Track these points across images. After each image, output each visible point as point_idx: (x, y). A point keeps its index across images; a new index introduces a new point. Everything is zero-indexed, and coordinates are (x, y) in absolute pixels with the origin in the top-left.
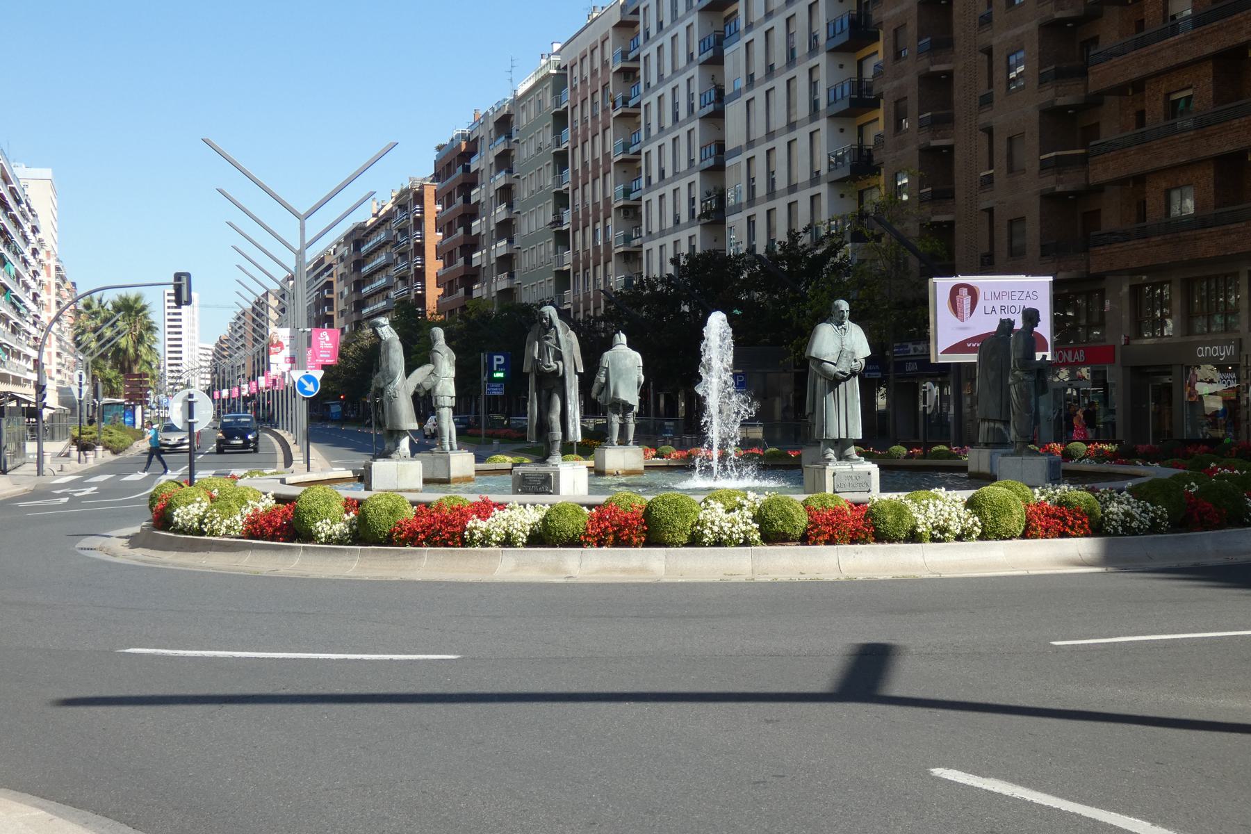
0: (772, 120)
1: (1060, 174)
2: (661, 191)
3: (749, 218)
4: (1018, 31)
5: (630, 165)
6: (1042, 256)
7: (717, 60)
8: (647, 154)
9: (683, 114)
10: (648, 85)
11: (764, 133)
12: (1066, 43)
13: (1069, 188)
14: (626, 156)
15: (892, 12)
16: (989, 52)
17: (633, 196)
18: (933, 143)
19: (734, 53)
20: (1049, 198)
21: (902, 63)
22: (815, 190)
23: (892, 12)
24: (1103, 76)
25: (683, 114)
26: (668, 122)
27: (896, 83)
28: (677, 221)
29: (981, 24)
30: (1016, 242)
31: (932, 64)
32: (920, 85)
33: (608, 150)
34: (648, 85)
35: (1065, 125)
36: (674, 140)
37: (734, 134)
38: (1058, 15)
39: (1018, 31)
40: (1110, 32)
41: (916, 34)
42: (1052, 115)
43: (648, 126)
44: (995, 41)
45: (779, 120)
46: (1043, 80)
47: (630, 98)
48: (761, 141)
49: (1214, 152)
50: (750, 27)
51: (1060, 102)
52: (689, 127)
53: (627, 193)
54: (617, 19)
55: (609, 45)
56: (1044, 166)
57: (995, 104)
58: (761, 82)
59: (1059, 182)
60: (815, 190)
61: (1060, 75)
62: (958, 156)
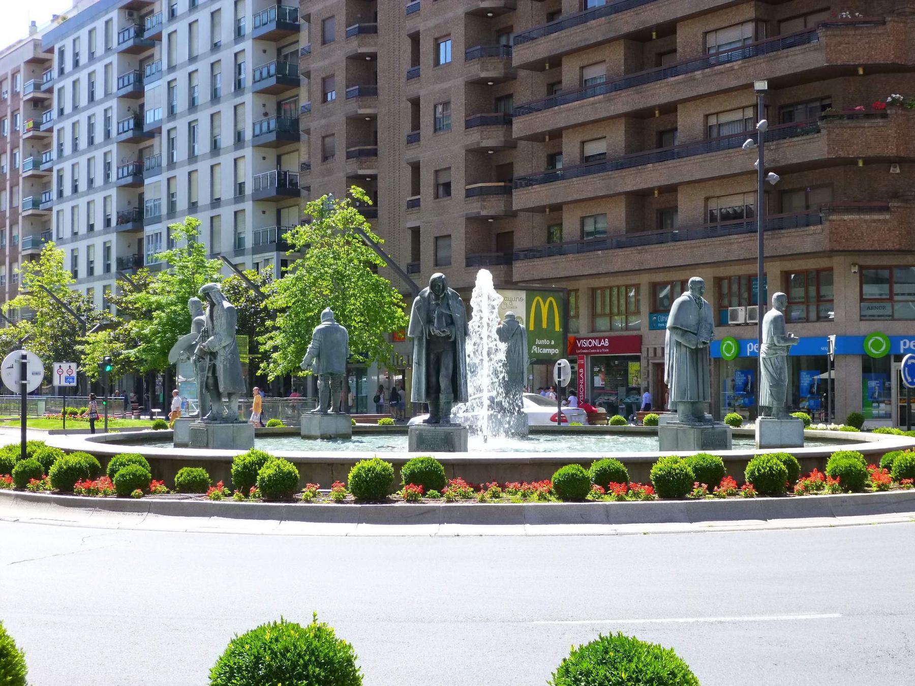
0: (195, 46)
1: (484, 201)
2: (75, 119)
3: (169, 83)
4: (446, 85)
5: (39, 181)
6: (467, 197)
7: (138, 93)
8: (60, 90)
9: (99, 137)
10: (61, 112)
11: (187, 58)
12: (489, 30)
13: (492, 213)
14: (36, 172)
15: (321, 64)
16: (415, 38)
17: (43, 167)
18: (361, 172)
19: (154, 90)
20: (473, 220)
21: (330, 106)
22: (239, 207)
23: (321, 64)
24: (522, 55)
25: (99, 137)
26: (83, 100)
27: (323, 122)
28: (91, 227)
29: (409, 78)
30: (442, 254)
31: (360, 108)
32: (347, 124)
33: (15, 205)
34: (61, 112)
35: (491, 102)
36: (90, 32)
37: (154, 115)
38: (483, 75)
39: (446, 85)
40: (527, 16)
41: (344, 83)
42: (477, 85)
43: (60, 145)
44: (422, 93)
45: (202, 44)
46: (469, 56)
47: (42, 123)
48: (183, 65)
49: (629, 188)
50: (171, 68)
51: (485, 144)
52: (107, 61)
53: (36, 204)
54: (30, 56)
55: (20, 78)
56: (469, 194)
57: (422, 142)
58: (184, 16)
59: (483, 207)
60: (239, 207)
61: (484, 122)
62: (381, 64)
